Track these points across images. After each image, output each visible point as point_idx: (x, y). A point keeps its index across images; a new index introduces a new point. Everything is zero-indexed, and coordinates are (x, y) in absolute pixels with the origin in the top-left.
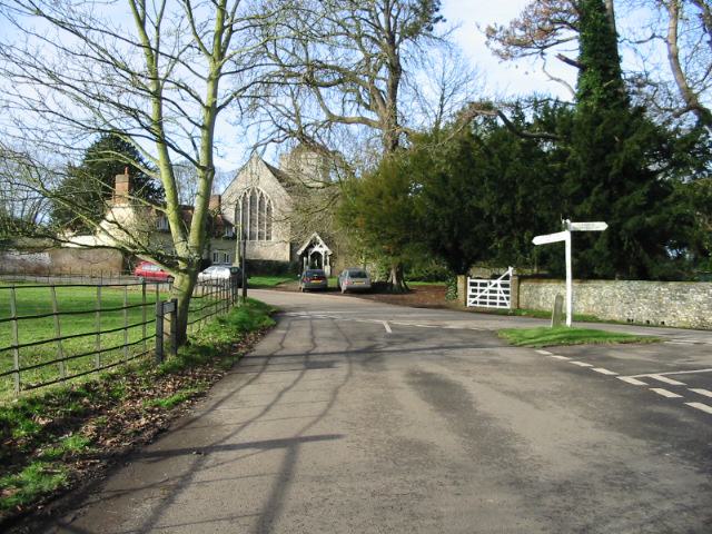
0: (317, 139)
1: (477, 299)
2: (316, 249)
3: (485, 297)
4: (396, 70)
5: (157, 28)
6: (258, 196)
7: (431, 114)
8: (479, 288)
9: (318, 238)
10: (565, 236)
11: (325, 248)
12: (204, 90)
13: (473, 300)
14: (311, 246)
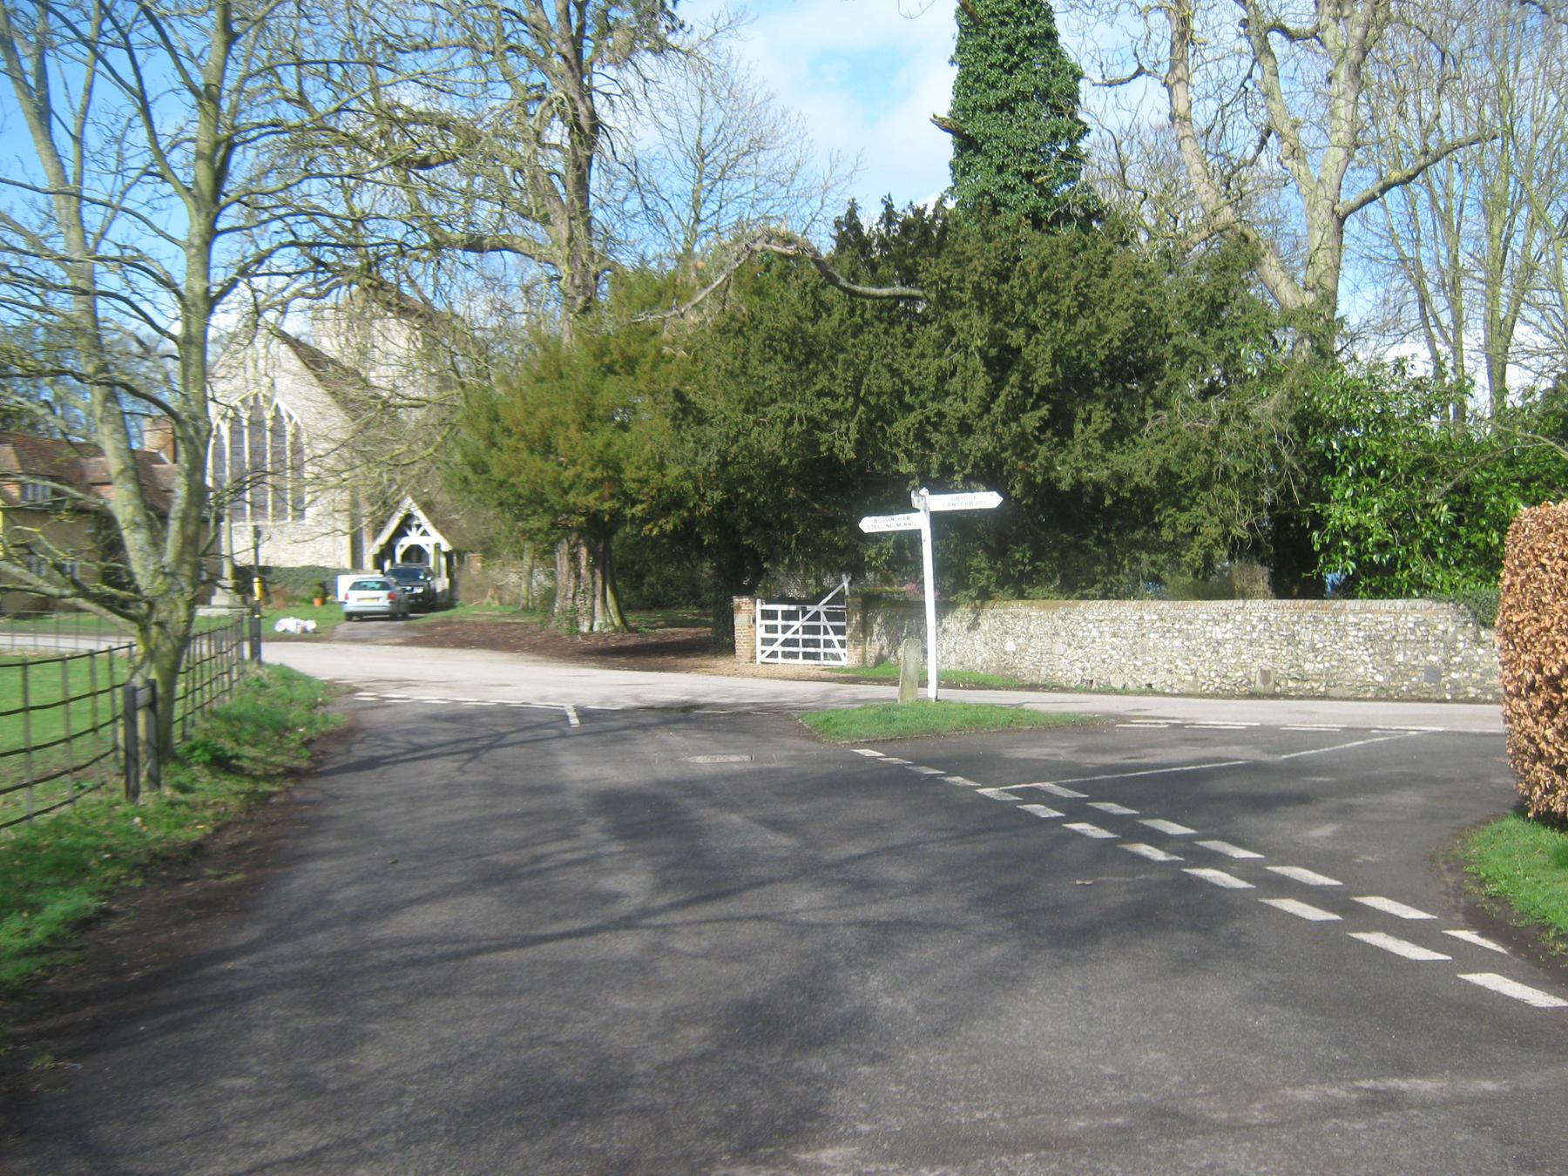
0: (406, 290)
1: (777, 647)
2: (412, 538)
3: (794, 643)
4: (587, 132)
5: (78, 140)
6: (268, 414)
7: (673, 224)
8: (780, 622)
9: (419, 513)
10: (918, 521)
11: (435, 537)
12: (177, 264)
13: (769, 649)
14: (401, 532)
